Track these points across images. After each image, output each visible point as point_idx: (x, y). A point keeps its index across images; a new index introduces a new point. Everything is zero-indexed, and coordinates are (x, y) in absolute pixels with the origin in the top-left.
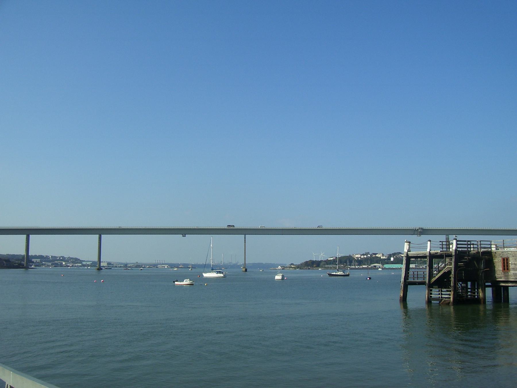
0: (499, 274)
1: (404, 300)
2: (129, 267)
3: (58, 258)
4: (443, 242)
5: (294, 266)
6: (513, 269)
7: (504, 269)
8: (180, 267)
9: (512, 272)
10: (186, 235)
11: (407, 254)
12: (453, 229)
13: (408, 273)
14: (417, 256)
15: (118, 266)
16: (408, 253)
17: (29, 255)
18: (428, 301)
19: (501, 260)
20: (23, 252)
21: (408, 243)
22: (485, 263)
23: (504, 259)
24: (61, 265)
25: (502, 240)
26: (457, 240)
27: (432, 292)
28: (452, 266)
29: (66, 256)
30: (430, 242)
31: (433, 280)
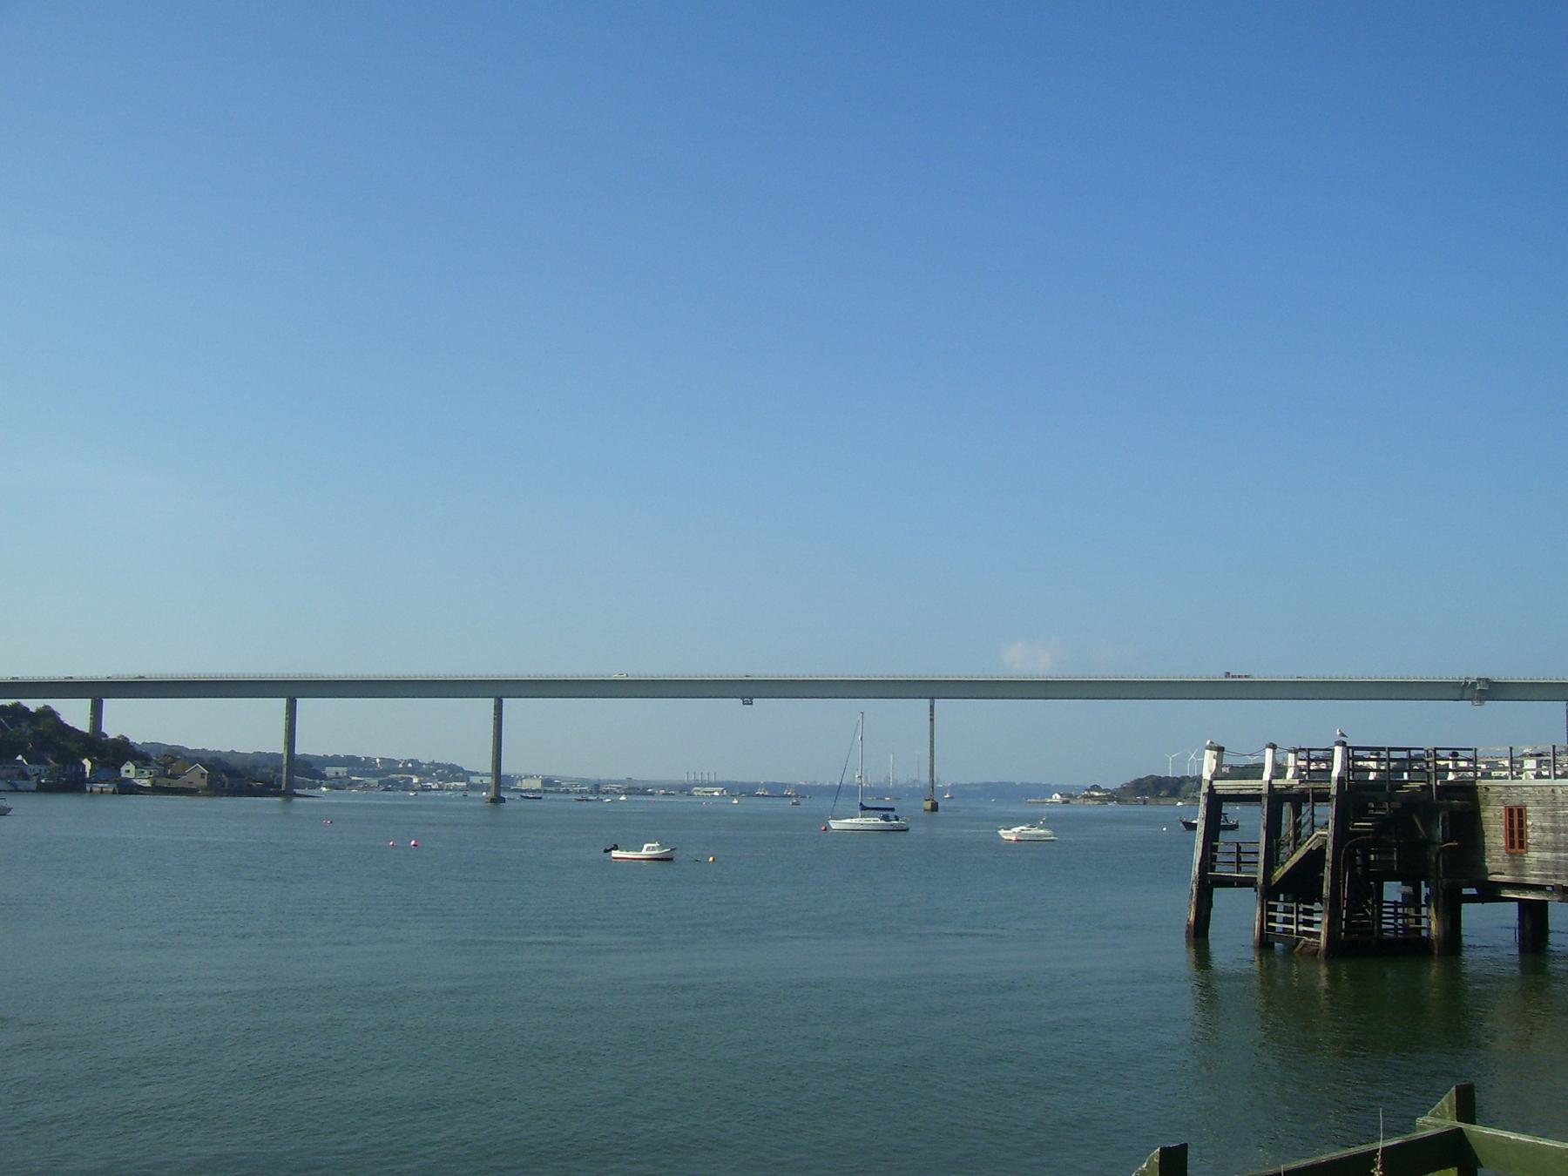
0: (1497, 860)
1: (1199, 931)
2: (607, 793)
3: (401, 766)
4: (1311, 752)
5: (1099, 792)
6: (1538, 844)
7: (1512, 845)
8: (758, 795)
9: (1533, 856)
10: (754, 700)
11: (1209, 787)
12: (1552, 683)
13: (1215, 849)
14: (1239, 795)
15: (456, 797)
16: (1215, 783)
17: (296, 753)
18: (1260, 943)
19: (1504, 814)
20: (279, 747)
21: (1215, 753)
22: (1447, 823)
23: (1510, 811)
24: (407, 786)
25: (1505, 749)
26: (1348, 745)
27: (1274, 914)
28: (1329, 833)
29: (425, 758)
30: (1271, 750)
31: (1279, 873)
